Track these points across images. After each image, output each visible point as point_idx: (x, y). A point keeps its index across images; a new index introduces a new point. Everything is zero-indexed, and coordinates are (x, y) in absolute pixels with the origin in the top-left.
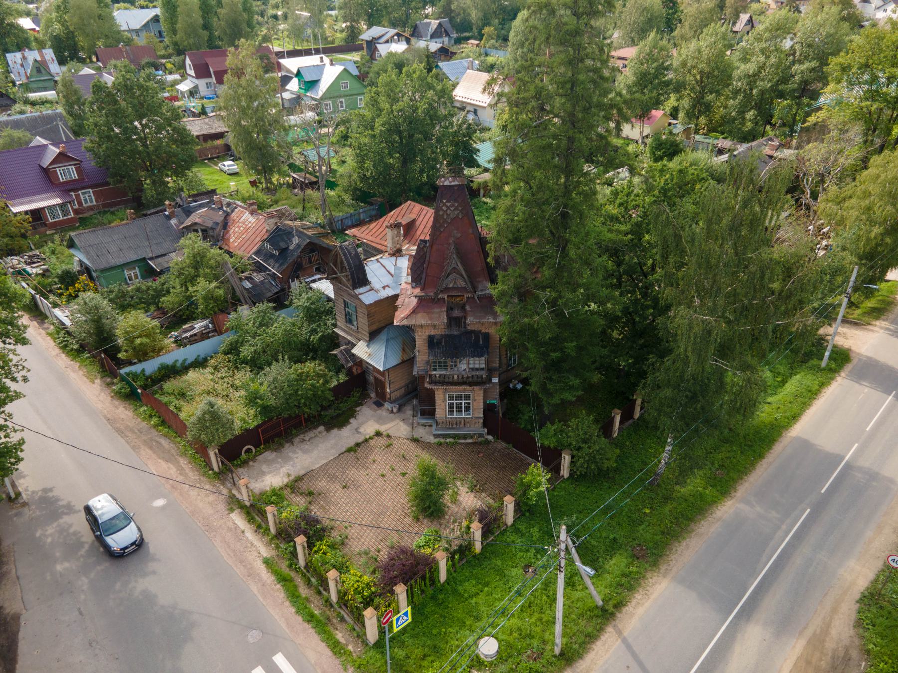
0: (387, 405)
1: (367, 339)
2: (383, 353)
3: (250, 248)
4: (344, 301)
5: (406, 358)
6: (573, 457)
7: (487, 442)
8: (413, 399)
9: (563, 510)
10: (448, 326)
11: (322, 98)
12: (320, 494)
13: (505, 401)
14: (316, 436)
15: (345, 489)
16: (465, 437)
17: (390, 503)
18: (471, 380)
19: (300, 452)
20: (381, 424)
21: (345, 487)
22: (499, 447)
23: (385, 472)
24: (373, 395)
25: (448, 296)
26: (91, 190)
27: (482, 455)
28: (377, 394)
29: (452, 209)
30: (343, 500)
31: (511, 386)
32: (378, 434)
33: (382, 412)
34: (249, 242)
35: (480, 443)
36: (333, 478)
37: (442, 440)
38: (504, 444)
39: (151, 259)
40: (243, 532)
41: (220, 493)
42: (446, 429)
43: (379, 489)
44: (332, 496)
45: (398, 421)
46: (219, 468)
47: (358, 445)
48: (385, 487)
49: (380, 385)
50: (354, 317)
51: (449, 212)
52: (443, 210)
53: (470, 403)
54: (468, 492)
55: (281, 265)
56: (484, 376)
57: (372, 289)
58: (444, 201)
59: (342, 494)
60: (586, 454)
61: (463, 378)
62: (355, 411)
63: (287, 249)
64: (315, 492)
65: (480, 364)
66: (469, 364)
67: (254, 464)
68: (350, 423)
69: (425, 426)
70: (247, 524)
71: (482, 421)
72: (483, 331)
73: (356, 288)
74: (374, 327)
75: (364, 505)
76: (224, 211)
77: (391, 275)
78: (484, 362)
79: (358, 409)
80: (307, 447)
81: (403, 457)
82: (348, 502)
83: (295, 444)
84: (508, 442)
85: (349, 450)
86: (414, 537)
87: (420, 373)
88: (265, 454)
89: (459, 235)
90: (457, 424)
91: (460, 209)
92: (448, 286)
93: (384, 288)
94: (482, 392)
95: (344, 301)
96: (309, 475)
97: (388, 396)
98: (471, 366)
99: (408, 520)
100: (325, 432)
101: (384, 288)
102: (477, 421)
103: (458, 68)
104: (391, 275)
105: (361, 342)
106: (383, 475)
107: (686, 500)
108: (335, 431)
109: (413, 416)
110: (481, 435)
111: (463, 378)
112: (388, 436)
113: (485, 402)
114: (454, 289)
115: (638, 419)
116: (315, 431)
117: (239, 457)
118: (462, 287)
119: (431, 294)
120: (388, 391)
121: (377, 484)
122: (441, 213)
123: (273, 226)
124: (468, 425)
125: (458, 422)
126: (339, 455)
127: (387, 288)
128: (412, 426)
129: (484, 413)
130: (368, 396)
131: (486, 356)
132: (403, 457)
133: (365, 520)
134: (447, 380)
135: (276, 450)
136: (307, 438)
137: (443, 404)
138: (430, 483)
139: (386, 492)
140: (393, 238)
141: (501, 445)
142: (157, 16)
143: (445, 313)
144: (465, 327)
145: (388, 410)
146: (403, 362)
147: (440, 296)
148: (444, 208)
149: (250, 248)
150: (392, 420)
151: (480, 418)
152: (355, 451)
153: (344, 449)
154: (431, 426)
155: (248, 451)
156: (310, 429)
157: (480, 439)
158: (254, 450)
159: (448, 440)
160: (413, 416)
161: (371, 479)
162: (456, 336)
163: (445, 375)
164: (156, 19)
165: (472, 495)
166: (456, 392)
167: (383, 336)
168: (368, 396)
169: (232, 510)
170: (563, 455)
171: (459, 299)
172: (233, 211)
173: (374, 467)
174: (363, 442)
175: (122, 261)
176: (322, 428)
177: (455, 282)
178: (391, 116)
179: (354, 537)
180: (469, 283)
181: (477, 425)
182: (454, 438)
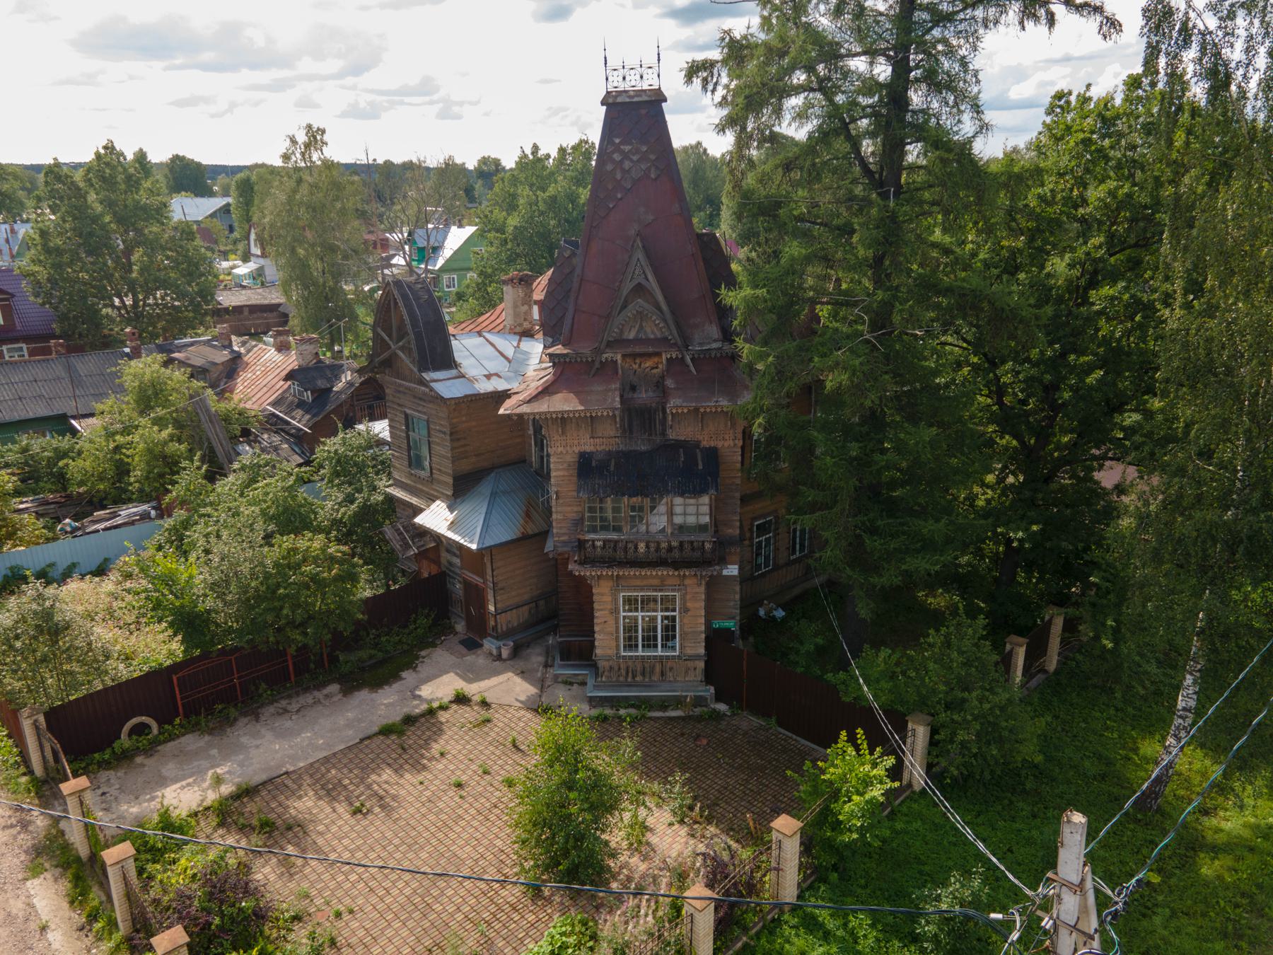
0: (489, 645)
1: (450, 493)
2: (483, 516)
3: (264, 398)
4: (406, 416)
5: (531, 529)
6: (934, 731)
7: (716, 716)
8: (548, 634)
9: (927, 868)
10: (624, 431)
11: (442, 269)
12: (289, 828)
13: (751, 639)
14: (317, 702)
15: (359, 816)
16: (663, 704)
17: (468, 849)
18: (676, 554)
19: (269, 735)
20: (470, 681)
21: (357, 811)
22: (745, 725)
23: (464, 778)
24: (460, 627)
25: (624, 356)
26: (24, 346)
27: (705, 742)
28: (470, 626)
29: (635, 158)
30: (346, 842)
31: (762, 612)
32: (461, 699)
33: (478, 659)
34: (265, 389)
35: (699, 719)
36: (330, 792)
37: (608, 712)
38: (756, 721)
39: (74, 417)
40: (44, 929)
41: (25, 825)
42: (620, 686)
43: (444, 817)
44: (321, 834)
45: (510, 674)
46: (46, 768)
47: (409, 720)
48: (460, 811)
49: (475, 595)
50: (425, 451)
51: (627, 165)
52: (613, 161)
53: (674, 618)
54: (671, 824)
55: (314, 416)
56: (708, 546)
57: (463, 376)
58: (617, 141)
59: (346, 829)
60: (976, 718)
61: (658, 549)
62: (417, 657)
63: (330, 390)
64: (279, 822)
65: (698, 514)
66: (671, 514)
67: (146, 761)
68: (401, 679)
69: (571, 684)
70: (66, 905)
71: (701, 665)
72: (705, 444)
73: (427, 369)
74: (466, 466)
75: (398, 855)
76: (233, 351)
77: (507, 358)
78: (706, 509)
79: (423, 653)
80: (288, 724)
81: (515, 746)
82: (358, 848)
83: (263, 718)
84: (766, 714)
85: (386, 731)
86: (522, 940)
87: (560, 550)
88: (183, 739)
89: (650, 218)
90: (643, 674)
91: (652, 157)
92: (625, 336)
93: (488, 377)
94: (702, 589)
95: (406, 416)
96: (276, 784)
97: (492, 623)
98: (678, 520)
99: (512, 894)
100: (340, 696)
101: (488, 377)
102: (690, 664)
103: (646, 915)
104: (507, 358)
105: (438, 502)
106: (459, 785)
107: (1251, 850)
108: (364, 694)
109: (546, 666)
110: (699, 701)
111: (658, 549)
112: (485, 704)
113: (708, 624)
114: (637, 341)
115: (1057, 672)
116: (316, 693)
117: (110, 744)
118: (656, 339)
119: (587, 351)
120: (492, 608)
121: (441, 805)
122: (609, 167)
123: (310, 357)
124: (670, 676)
125: (646, 669)
126: (362, 740)
127: (495, 377)
128: (542, 685)
129: (707, 648)
130: (450, 630)
131: (712, 492)
132: (515, 746)
133: (395, 892)
134: (620, 554)
135: (211, 732)
136: (294, 706)
137: (612, 622)
138: (570, 785)
139: (463, 823)
140: (515, 306)
141: (748, 722)
142: (228, 205)
143: (617, 393)
144: (663, 433)
145: (491, 654)
146: (524, 539)
147: (607, 355)
148: (617, 157)
149: (264, 398)
150: (497, 673)
151: (697, 657)
152: (401, 733)
153: (376, 729)
154: (583, 684)
155: (140, 730)
156: (307, 690)
157: (698, 710)
158: (155, 730)
159: (622, 712)
160: (546, 666)
161: (428, 793)
162: (642, 453)
163: (616, 542)
164: (226, 210)
165: (684, 831)
166: (642, 589)
167: (486, 488)
168: (450, 630)
169: (34, 870)
170: (910, 725)
171: (648, 364)
172: (249, 351)
173: (440, 766)
174: (423, 715)
175: (16, 416)
176: (334, 688)
177: (641, 327)
178: (534, 208)
179: (354, 940)
180: (673, 327)
181: (691, 677)
182: (637, 707)
